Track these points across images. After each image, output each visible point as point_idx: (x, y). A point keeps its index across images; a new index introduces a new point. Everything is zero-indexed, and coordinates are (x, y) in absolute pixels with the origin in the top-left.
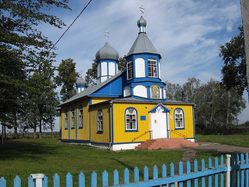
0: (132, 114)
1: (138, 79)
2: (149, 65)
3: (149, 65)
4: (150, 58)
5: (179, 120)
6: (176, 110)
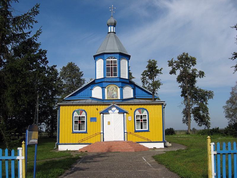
0: (81, 116)
4: (108, 58)
5: (142, 121)
6: (137, 111)
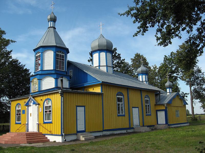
1: (45, 72)
2: (57, 58)
3: (57, 58)
